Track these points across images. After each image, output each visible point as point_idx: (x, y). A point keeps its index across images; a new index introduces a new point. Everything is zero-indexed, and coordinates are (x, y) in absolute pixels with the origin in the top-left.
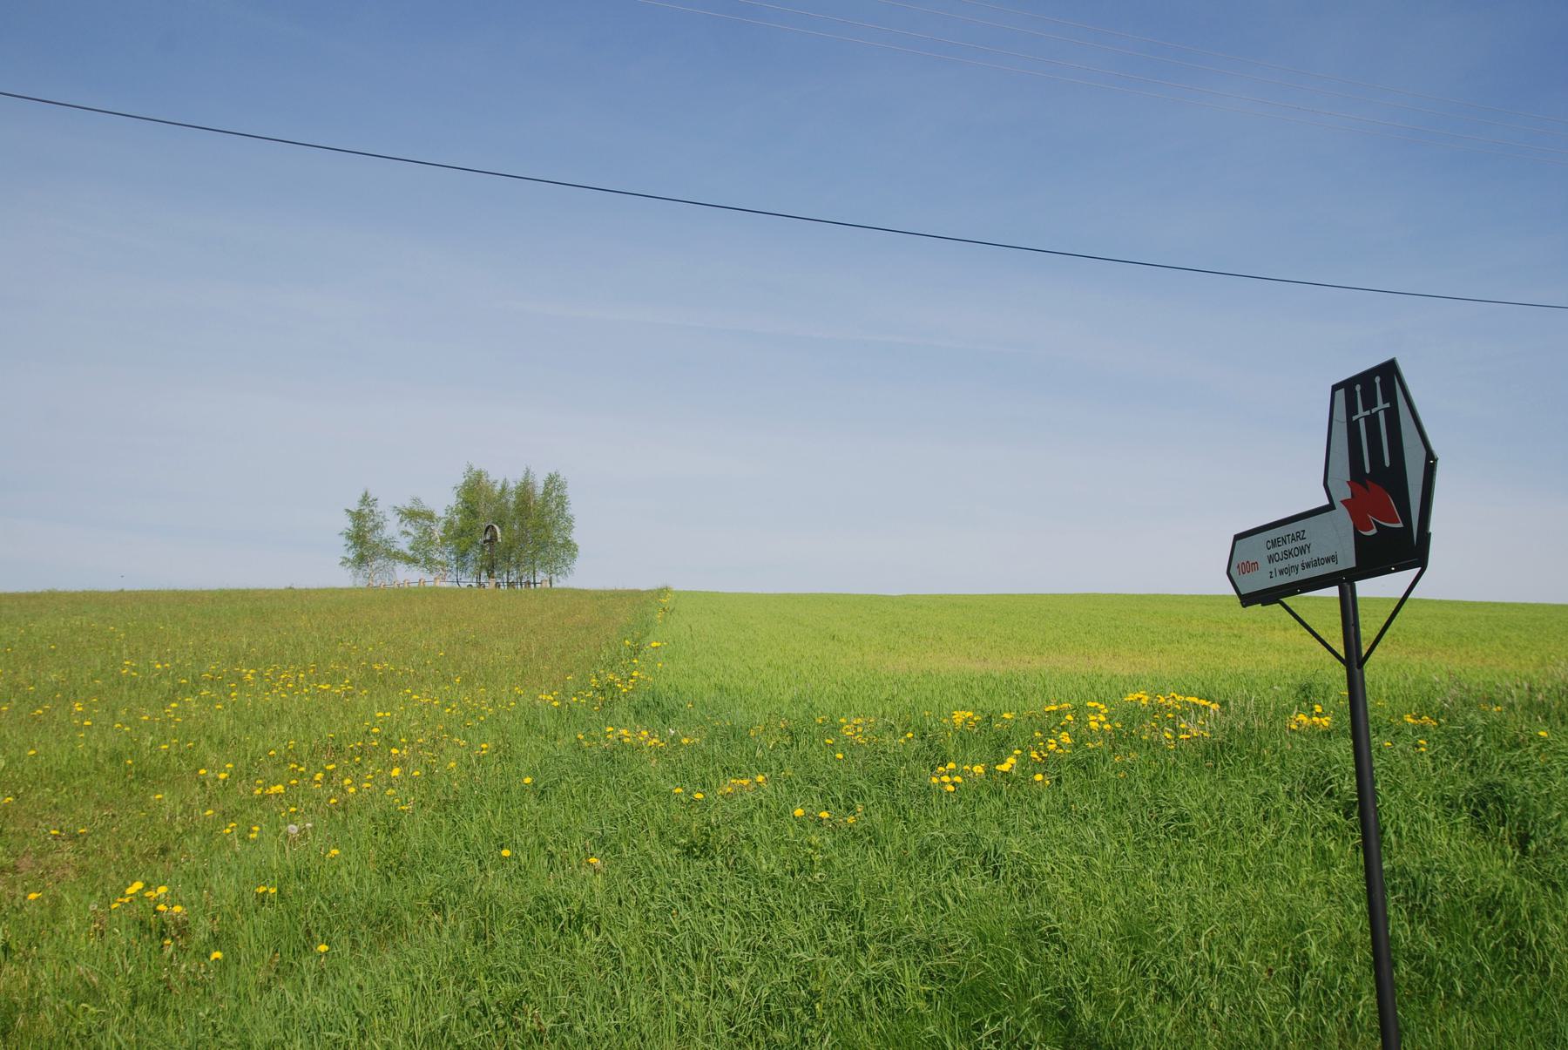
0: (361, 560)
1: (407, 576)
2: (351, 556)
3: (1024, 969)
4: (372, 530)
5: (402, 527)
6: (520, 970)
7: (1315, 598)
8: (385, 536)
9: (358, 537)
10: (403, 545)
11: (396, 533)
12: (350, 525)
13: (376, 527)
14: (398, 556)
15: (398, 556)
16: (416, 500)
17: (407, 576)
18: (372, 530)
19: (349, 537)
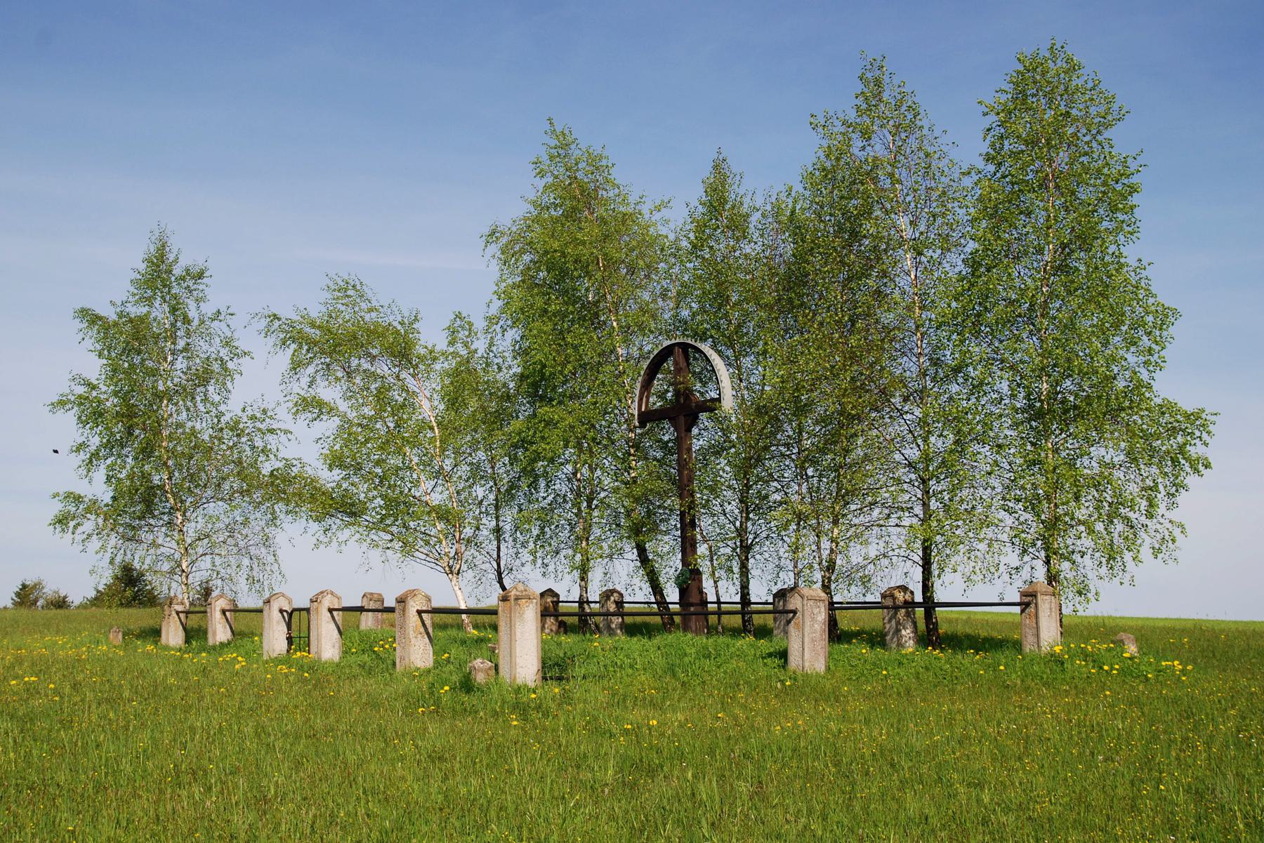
0: (140, 504)
1: (322, 566)
2: (99, 489)
3: (1061, 154)
4: (183, 392)
5: (300, 387)
6: (1154, 346)
7: (975, 613)
8: (232, 408)
9: (128, 414)
10: (305, 447)
11: (270, 399)
12: (94, 367)
13: (203, 378)
14: (287, 490)
15: (287, 490)
16: (347, 290)
17: (322, 566)
18: (183, 392)
19: (93, 414)
